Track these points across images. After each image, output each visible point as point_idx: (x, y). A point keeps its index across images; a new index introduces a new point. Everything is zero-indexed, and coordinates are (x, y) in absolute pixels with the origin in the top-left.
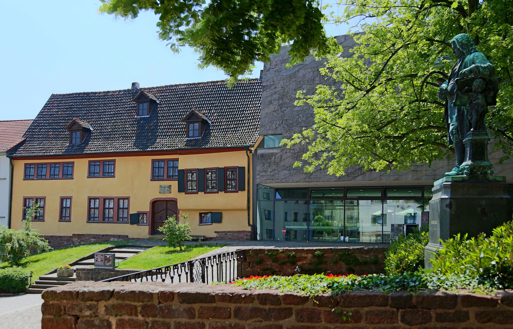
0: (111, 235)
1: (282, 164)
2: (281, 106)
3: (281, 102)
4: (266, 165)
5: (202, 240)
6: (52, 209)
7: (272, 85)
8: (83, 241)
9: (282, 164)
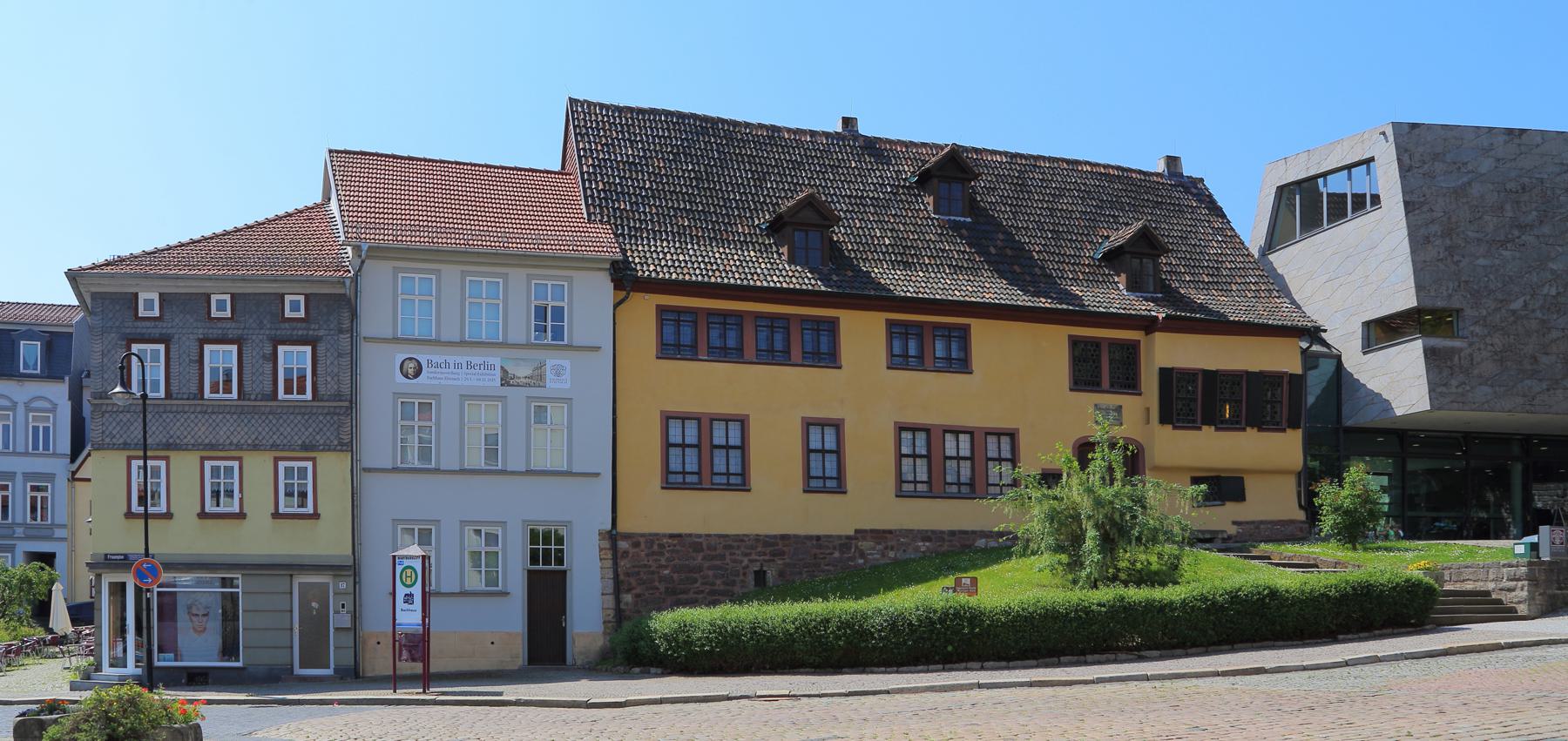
0: (974, 532)
1: (1476, 372)
2: (1450, 250)
3: (1448, 242)
4: (1446, 373)
5: (1224, 540)
6: (776, 454)
7: (1423, 204)
8: (892, 548)
9: (1476, 372)
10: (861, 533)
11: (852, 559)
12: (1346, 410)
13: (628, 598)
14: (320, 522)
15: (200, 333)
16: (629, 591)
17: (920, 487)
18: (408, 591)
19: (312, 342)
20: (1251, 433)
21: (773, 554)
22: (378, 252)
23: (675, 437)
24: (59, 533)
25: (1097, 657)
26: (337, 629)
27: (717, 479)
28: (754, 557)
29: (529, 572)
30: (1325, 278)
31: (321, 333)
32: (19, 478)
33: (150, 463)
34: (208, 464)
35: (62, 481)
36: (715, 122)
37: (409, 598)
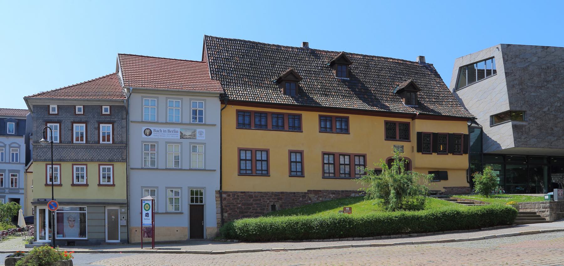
0: (350, 191)
1: (531, 134)
2: (522, 90)
3: (521, 87)
4: (520, 134)
5: (440, 194)
6: (279, 163)
7: (512, 73)
8: (321, 197)
9: (531, 134)
10: (310, 191)
11: (307, 201)
12: (484, 147)
13: (226, 215)
14: (115, 187)
15: (72, 120)
16: (226, 212)
17: (331, 175)
18: (147, 212)
19: (112, 123)
20: (450, 155)
21: (278, 199)
22: (136, 91)
23: (243, 157)
24: (21, 191)
25: (394, 236)
26: (121, 226)
27: (258, 172)
28: (271, 200)
29: (190, 205)
30: (476, 100)
31: (116, 119)
32: (7, 172)
33: (54, 166)
34: (75, 167)
35: (22, 173)
36: (257, 44)
37: (147, 215)
